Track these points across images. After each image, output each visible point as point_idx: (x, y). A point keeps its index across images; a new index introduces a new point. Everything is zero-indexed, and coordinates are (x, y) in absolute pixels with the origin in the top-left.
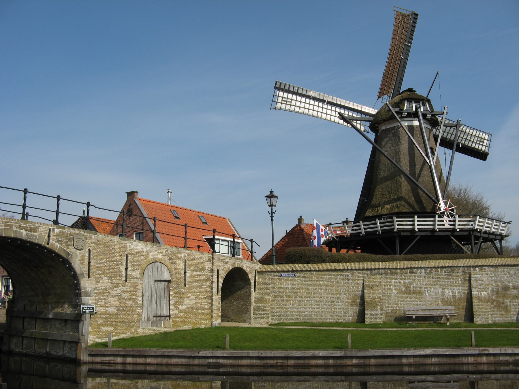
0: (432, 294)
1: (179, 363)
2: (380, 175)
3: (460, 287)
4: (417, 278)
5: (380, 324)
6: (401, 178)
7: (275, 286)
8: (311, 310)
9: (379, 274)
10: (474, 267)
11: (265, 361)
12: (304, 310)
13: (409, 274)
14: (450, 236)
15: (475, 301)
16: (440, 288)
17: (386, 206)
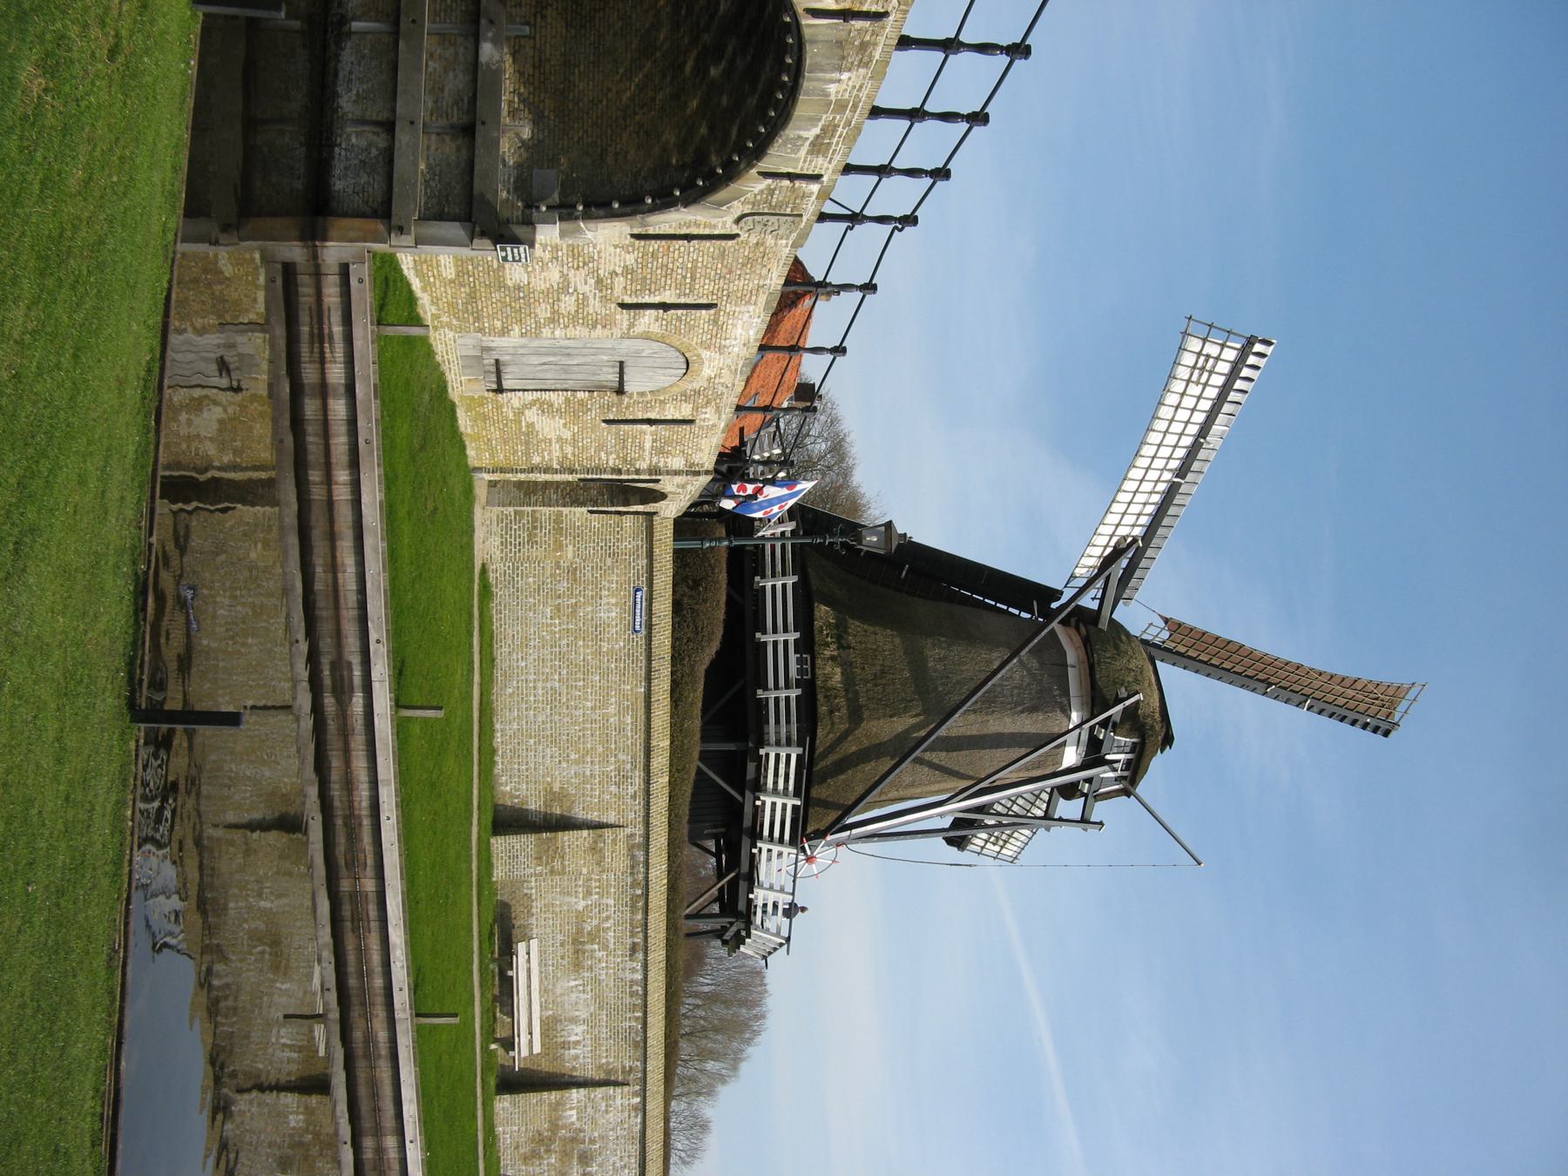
0: (573, 996)
1: (340, 575)
2: (934, 645)
3: (589, 1060)
4: (619, 960)
5: (491, 875)
6: (917, 715)
7: (605, 571)
8: (532, 677)
9: (632, 867)
10: (643, 1094)
11: (366, 822)
12: (532, 657)
13: (629, 941)
14: (737, 871)
15: (553, 1097)
16: (588, 1014)
17: (838, 670)
